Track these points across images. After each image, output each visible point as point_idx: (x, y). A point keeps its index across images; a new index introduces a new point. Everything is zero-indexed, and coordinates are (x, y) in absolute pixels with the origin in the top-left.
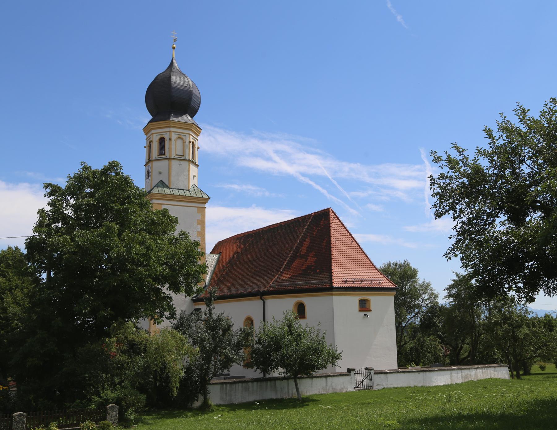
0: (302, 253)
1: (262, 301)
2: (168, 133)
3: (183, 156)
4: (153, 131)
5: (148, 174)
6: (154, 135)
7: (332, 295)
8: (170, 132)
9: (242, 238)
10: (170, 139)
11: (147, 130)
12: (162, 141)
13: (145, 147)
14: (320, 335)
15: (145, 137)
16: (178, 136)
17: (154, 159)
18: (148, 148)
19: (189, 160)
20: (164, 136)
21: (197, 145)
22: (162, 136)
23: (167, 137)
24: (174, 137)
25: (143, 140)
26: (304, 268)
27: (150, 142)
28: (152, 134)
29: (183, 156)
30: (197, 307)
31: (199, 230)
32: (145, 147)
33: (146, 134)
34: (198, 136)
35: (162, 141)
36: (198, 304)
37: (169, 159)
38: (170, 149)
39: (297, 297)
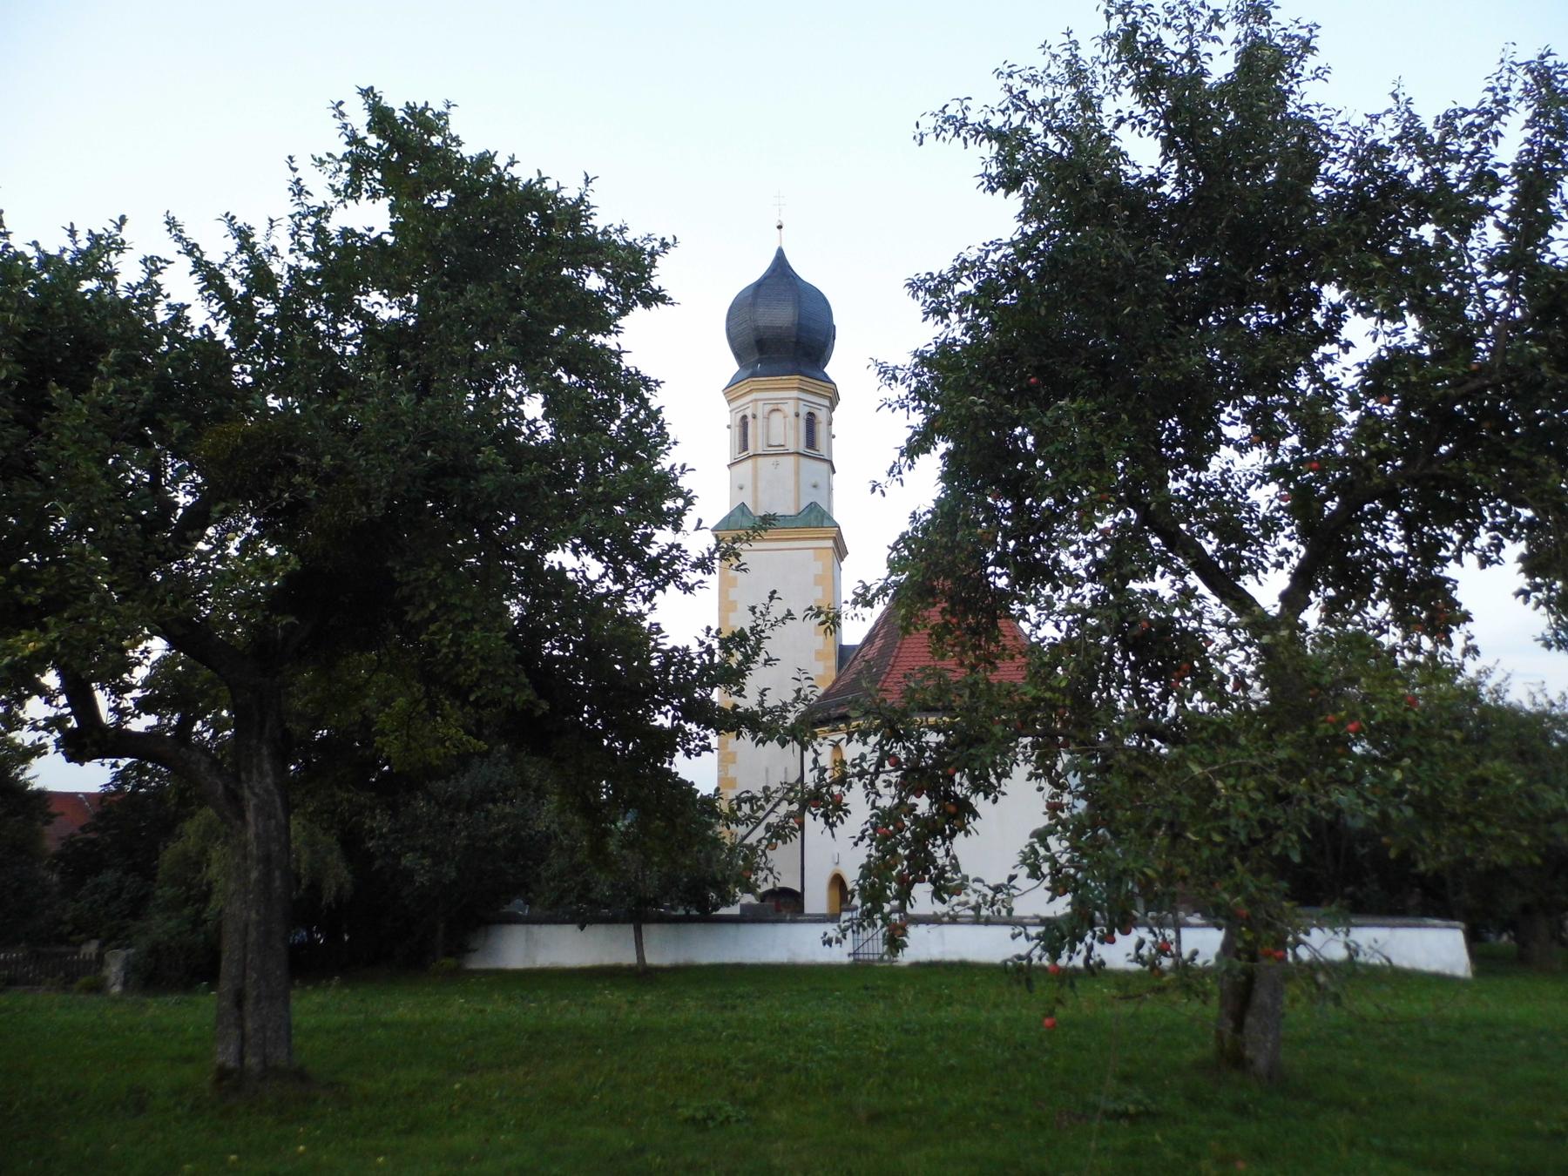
23: (749, 413)
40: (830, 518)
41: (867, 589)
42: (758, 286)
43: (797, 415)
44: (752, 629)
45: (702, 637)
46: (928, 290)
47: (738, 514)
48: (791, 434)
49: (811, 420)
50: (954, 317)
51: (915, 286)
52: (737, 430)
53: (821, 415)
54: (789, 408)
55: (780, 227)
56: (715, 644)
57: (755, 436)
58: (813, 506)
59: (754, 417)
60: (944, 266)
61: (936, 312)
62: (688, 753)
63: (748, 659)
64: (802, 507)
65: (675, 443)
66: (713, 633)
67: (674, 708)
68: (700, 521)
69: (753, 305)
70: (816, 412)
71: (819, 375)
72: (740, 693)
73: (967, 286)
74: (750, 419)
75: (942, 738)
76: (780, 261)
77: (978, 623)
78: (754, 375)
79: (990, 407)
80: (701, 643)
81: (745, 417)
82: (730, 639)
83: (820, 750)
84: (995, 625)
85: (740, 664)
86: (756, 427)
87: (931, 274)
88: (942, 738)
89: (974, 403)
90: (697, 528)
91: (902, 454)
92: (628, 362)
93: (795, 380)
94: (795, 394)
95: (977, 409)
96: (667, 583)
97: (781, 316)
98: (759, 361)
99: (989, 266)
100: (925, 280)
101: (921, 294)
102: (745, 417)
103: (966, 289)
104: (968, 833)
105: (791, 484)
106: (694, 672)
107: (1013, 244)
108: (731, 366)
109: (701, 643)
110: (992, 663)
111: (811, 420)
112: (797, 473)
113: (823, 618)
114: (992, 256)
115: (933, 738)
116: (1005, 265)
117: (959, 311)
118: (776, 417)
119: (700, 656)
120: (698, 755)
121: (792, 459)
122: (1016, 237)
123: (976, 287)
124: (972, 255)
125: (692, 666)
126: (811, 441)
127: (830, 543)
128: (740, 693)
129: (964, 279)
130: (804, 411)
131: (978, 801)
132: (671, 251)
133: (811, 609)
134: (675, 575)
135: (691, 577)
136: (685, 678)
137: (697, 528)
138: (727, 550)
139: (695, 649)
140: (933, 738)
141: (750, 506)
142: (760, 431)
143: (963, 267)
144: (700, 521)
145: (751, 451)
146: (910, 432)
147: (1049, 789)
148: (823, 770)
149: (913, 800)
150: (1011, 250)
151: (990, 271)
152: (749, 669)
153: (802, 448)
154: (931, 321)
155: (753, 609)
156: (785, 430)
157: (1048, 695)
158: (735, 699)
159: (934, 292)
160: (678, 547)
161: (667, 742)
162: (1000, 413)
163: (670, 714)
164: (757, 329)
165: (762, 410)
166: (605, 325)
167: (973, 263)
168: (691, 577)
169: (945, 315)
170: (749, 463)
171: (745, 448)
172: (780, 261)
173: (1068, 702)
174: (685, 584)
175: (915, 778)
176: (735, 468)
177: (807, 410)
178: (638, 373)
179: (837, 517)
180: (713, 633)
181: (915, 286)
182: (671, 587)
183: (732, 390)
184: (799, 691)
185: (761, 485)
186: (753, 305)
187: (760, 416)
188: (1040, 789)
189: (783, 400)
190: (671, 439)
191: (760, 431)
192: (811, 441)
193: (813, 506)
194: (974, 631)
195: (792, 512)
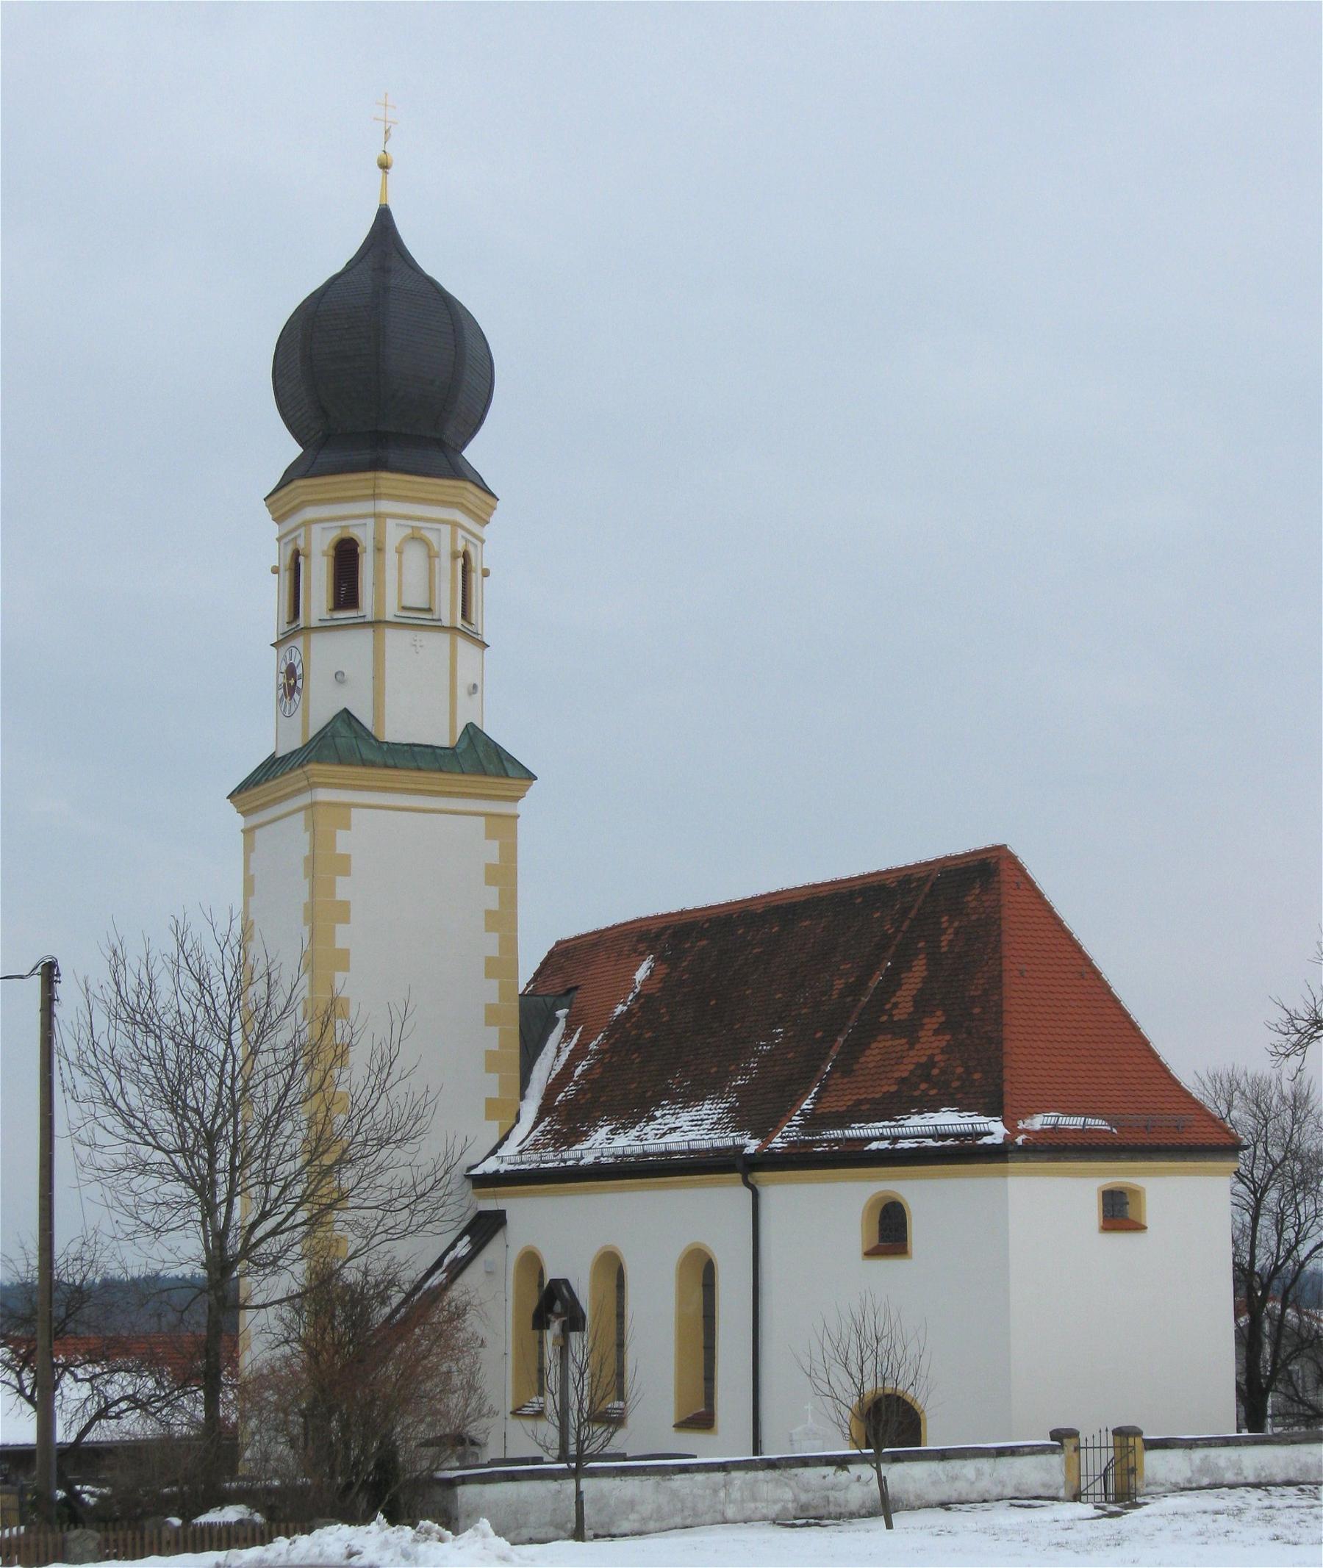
0: (899, 1015)
1: (749, 1192)
2: (370, 522)
3: (429, 610)
4: (310, 513)
5: (291, 682)
6: (316, 529)
7: (1004, 1174)
8: (377, 516)
9: (658, 936)
10: (379, 549)
11: (282, 497)
12: (346, 557)
13: (275, 570)
14: (1230, 1067)
15: (274, 529)
16: (409, 531)
17: (315, 623)
18: (286, 576)
19: (453, 629)
20: (356, 533)
21: (475, 562)
22: (345, 535)
23: (301, 544)
24: (394, 534)
25: (263, 542)
26: (904, 1070)
27: (296, 554)
28: (307, 524)
29: (429, 610)
30: (489, 1205)
31: (494, 905)
32: (275, 570)
33: (278, 519)
34: (483, 522)
35: (346, 557)
36: (495, 1196)
37: (377, 624)
38: (379, 583)
39: (871, 1178)
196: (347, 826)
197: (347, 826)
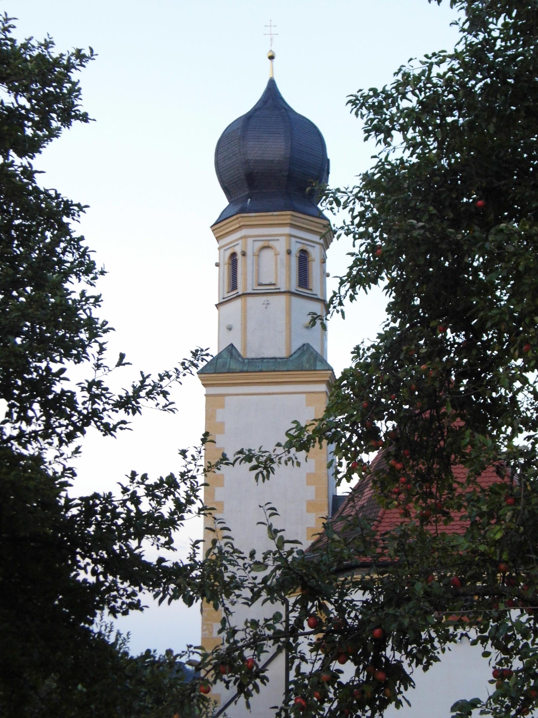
23: (238, 250)
40: (324, 361)
41: (301, 430)
42: (247, 120)
43: (289, 252)
44: (182, 475)
45: (126, 482)
46: (372, 107)
47: (225, 355)
48: (283, 272)
49: (304, 258)
50: (397, 137)
51: (358, 102)
52: (226, 268)
53: (315, 252)
54: (281, 245)
55: (271, 58)
56: (141, 491)
57: (245, 274)
58: (305, 349)
59: (244, 254)
60: (386, 81)
61: (378, 129)
62: (113, 612)
63: (180, 507)
64: (294, 348)
65: (102, 273)
66: (138, 478)
67: (95, 562)
68: (122, 356)
69: (243, 137)
70: (309, 249)
71: (312, 211)
72: (169, 544)
73: (411, 102)
74: (239, 257)
75: (368, 596)
76: (272, 89)
77: (430, 469)
78: (243, 210)
79: (432, 230)
80: (125, 490)
81: (234, 255)
82: (157, 486)
83: (232, 608)
84: (449, 472)
85: (172, 514)
86: (245, 265)
87: (374, 90)
88: (368, 596)
89: (412, 226)
90: (120, 364)
91: (342, 283)
92: (41, 182)
93: (287, 216)
94: (287, 230)
95: (415, 233)
96: (88, 424)
97: (272, 149)
98: (248, 196)
99: (435, 80)
100: (369, 97)
101: (364, 111)
102: (234, 255)
103: (409, 105)
104: (399, 704)
105: (282, 322)
106: (120, 522)
107: (456, 56)
108: (222, 202)
109: (125, 490)
110: (446, 514)
111: (304, 258)
112: (289, 312)
113: (254, 463)
114: (436, 70)
115: (358, 596)
116: (450, 79)
117: (404, 129)
118: (267, 255)
119: (123, 503)
120: (125, 613)
121: (282, 300)
122: (461, 48)
123: (420, 102)
124: (416, 69)
125: (117, 516)
126: (304, 279)
127: (323, 388)
128: (169, 544)
129: (409, 95)
130: (296, 248)
131: (416, 672)
132: (89, 64)
133: (241, 452)
134: (95, 414)
135: (113, 417)
136: (109, 528)
137: (120, 364)
138: (155, 387)
139: (118, 496)
140: (358, 596)
141: (238, 347)
142: (250, 268)
143: (406, 82)
144: (122, 356)
145: (240, 290)
146: (351, 260)
147: (496, 654)
148: (233, 632)
149: (335, 665)
150: (456, 64)
151: (435, 85)
152: (182, 518)
153: (294, 286)
154: (373, 139)
155: (183, 453)
156: (276, 268)
157: (482, 548)
158: (164, 553)
159: (378, 109)
160: (98, 384)
161: (90, 599)
162: (445, 237)
163: (89, 568)
164: (247, 162)
165: (252, 247)
166: (31, 147)
167: (417, 79)
168: (113, 417)
169: (388, 133)
170: (238, 303)
171: (234, 286)
172: (272, 89)
173: (505, 557)
174: (106, 425)
175: (338, 642)
176: (223, 308)
177: (299, 246)
178: (58, 196)
179: (329, 362)
180: (138, 478)
181: (358, 102)
182: (91, 429)
183: (221, 227)
184: (214, 542)
185: (251, 325)
186: (243, 137)
187: (249, 252)
188: (486, 654)
189: (275, 238)
190: (98, 268)
191: (250, 268)
192: (304, 279)
193: (305, 349)
194: (425, 478)
195: (282, 353)
196: (222, 406)
197: (222, 406)
